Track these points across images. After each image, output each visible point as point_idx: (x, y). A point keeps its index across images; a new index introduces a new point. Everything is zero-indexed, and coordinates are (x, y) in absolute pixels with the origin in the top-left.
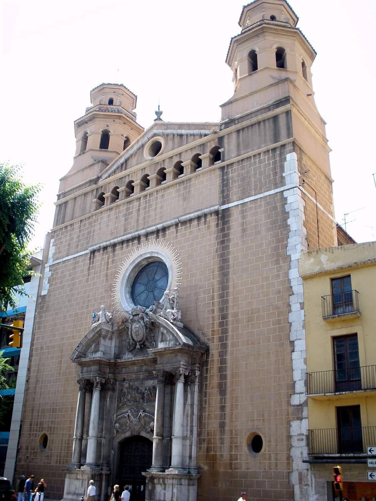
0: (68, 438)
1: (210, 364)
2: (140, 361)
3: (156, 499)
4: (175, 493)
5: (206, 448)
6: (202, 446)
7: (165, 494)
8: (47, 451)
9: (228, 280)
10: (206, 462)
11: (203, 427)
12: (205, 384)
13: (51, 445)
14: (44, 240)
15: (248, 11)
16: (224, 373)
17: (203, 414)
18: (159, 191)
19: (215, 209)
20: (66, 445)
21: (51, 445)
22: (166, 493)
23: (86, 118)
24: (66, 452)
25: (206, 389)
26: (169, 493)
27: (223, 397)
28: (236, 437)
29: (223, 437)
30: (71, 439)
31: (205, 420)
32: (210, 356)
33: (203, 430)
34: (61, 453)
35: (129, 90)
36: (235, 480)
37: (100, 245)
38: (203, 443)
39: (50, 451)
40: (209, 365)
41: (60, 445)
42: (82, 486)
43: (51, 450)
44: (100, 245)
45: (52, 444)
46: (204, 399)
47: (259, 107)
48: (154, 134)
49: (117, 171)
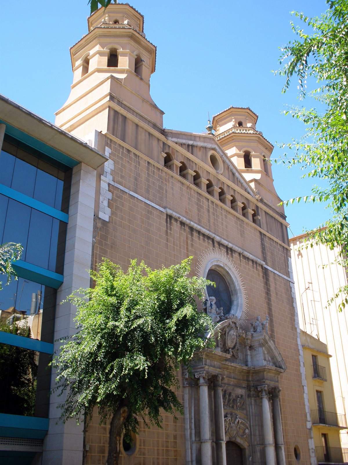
0: (166, 439)
2: (233, 368)
8: (138, 456)
13: (142, 447)
15: (248, 113)
19: (201, 229)
20: (165, 449)
21: (142, 447)
23: (144, 42)
24: (165, 457)
28: (144, 448)
30: (169, 440)
34: (158, 458)
35: (269, 143)
37: (181, 217)
39: (142, 456)
41: (156, 448)
43: (144, 454)
44: (181, 217)
45: (144, 445)
47: (146, 117)
48: (215, 148)
49: (184, 146)
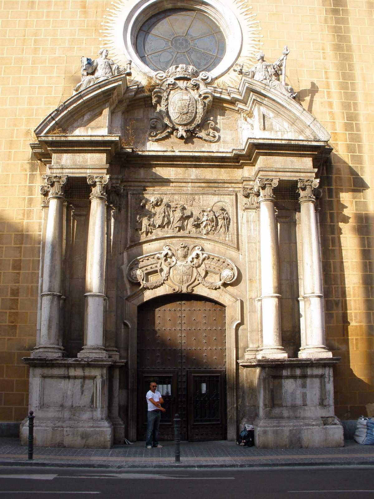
1: (336, 183)
3: (284, 404)
4: (329, 391)
5: (341, 315)
6: (334, 312)
7: (304, 395)
9: (351, 67)
10: (342, 338)
11: (333, 283)
12: (328, 213)
14: (136, 56)
16: (362, 200)
17: (331, 261)
18: (324, 56)
22: (307, 392)
25: (332, 221)
26: (314, 393)
27: (366, 237)
29: (370, 298)
31: (335, 271)
32: (334, 171)
33: (333, 286)
36: (53, 363)
38: (335, 307)
40: (334, 183)
42: (82, 392)
46: (330, 237)
